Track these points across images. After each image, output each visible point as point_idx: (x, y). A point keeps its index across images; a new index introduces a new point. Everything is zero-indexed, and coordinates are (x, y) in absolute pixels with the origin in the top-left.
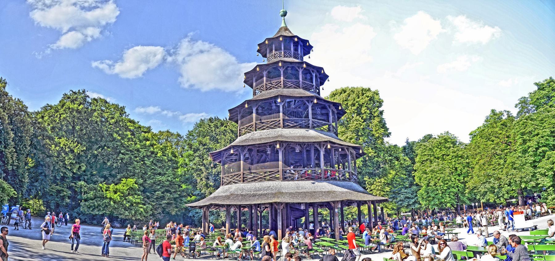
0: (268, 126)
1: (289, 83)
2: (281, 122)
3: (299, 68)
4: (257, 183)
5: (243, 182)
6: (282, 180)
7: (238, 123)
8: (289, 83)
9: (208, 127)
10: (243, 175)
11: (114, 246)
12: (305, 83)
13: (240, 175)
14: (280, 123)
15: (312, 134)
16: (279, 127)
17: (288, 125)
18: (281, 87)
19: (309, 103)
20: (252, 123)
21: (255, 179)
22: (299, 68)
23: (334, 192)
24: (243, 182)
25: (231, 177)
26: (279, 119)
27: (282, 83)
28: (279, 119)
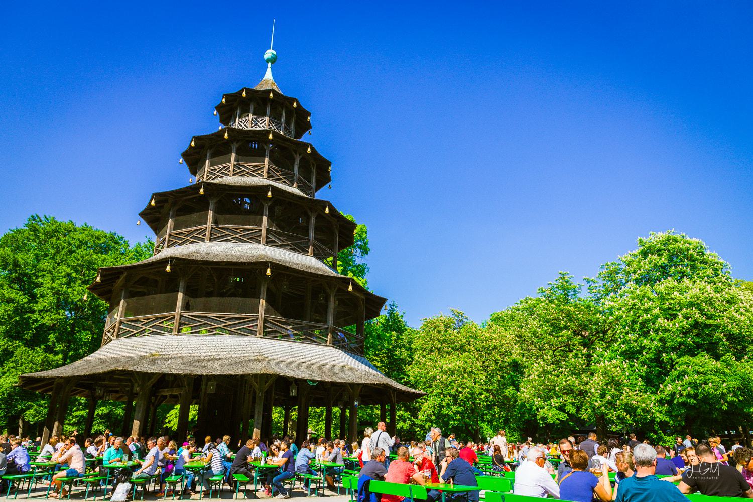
0: (237, 236)
1: (278, 174)
2: (264, 233)
3: (296, 154)
4: (210, 338)
5: (178, 332)
6: (262, 337)
7: (728, 448)
8: (278, 174)
9: (538, 312)
10: (180, 319)
11: (314, 197)
12: (302, 180)
13: (174, 318)
14: (261, 236)
15: (307, 261)
16: (259, 242)
17: (274, 242)
18: (262, 176)
19: (311, 212)
20: (203, 227)
21: (228, 240)
22: (296, 154)
23: (355, 370)
24: (178, 332)
25: (146, 321)
26: (259, 228)
27: (265, 169)
28: (259, 228)
